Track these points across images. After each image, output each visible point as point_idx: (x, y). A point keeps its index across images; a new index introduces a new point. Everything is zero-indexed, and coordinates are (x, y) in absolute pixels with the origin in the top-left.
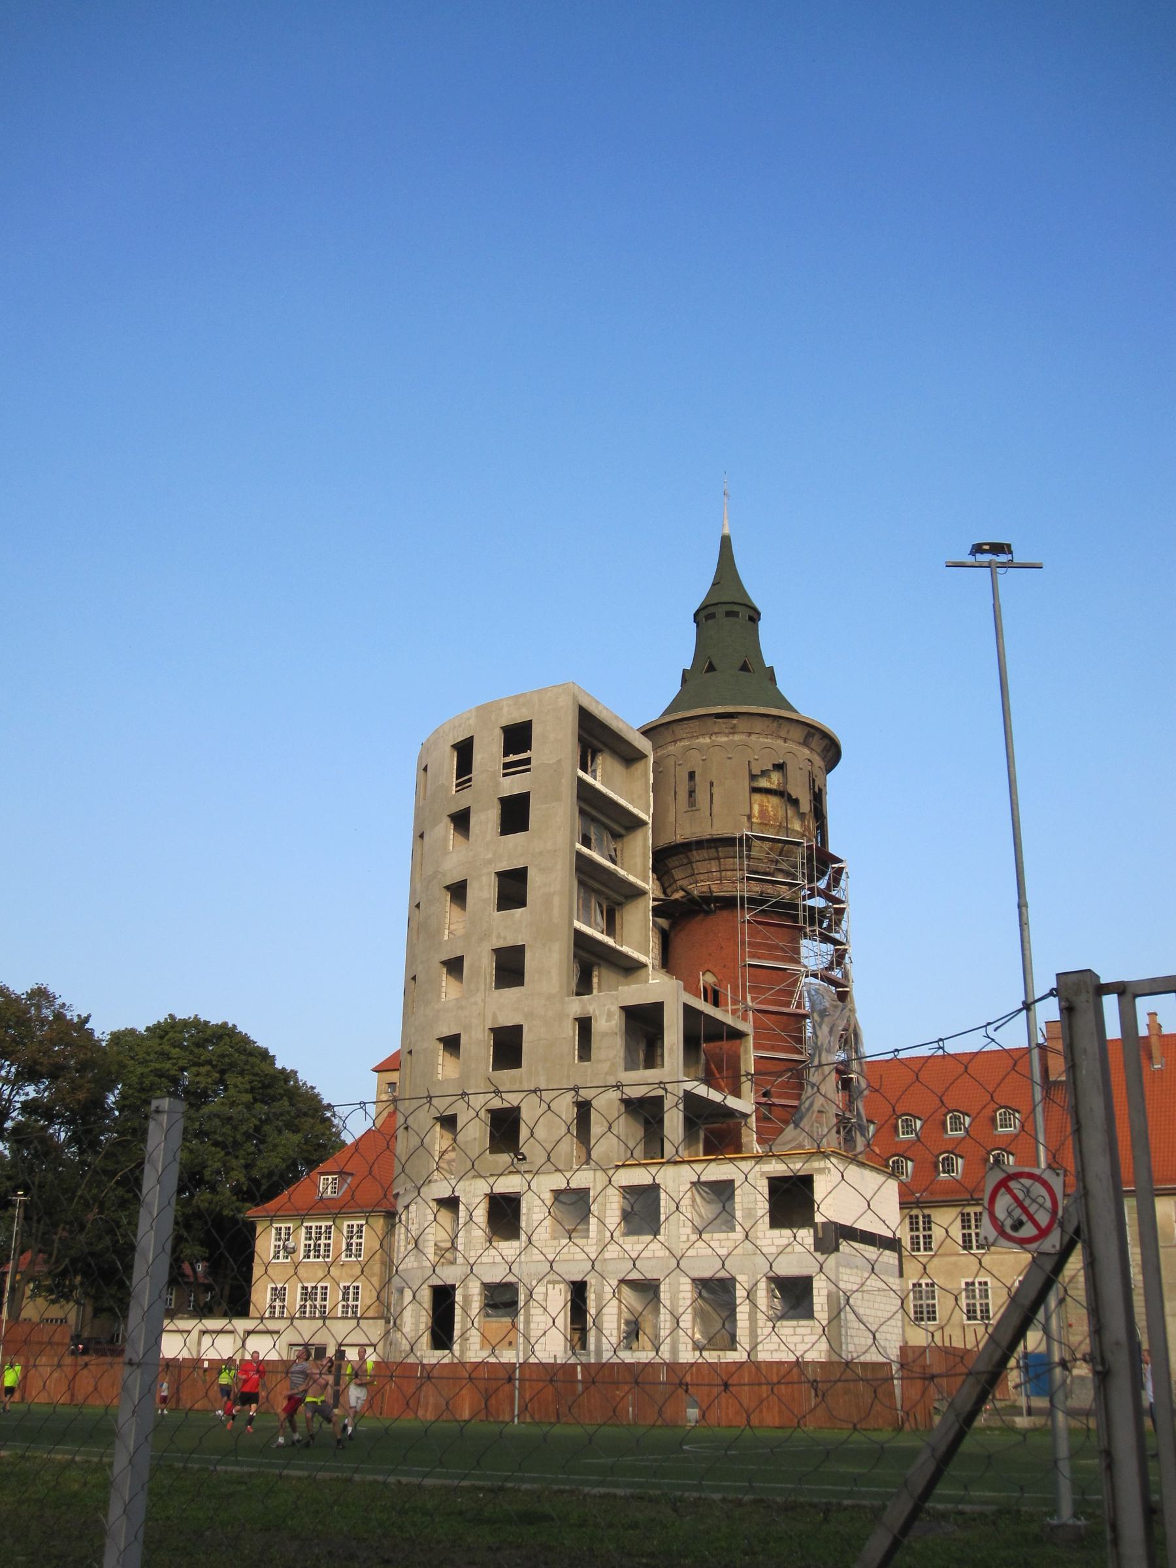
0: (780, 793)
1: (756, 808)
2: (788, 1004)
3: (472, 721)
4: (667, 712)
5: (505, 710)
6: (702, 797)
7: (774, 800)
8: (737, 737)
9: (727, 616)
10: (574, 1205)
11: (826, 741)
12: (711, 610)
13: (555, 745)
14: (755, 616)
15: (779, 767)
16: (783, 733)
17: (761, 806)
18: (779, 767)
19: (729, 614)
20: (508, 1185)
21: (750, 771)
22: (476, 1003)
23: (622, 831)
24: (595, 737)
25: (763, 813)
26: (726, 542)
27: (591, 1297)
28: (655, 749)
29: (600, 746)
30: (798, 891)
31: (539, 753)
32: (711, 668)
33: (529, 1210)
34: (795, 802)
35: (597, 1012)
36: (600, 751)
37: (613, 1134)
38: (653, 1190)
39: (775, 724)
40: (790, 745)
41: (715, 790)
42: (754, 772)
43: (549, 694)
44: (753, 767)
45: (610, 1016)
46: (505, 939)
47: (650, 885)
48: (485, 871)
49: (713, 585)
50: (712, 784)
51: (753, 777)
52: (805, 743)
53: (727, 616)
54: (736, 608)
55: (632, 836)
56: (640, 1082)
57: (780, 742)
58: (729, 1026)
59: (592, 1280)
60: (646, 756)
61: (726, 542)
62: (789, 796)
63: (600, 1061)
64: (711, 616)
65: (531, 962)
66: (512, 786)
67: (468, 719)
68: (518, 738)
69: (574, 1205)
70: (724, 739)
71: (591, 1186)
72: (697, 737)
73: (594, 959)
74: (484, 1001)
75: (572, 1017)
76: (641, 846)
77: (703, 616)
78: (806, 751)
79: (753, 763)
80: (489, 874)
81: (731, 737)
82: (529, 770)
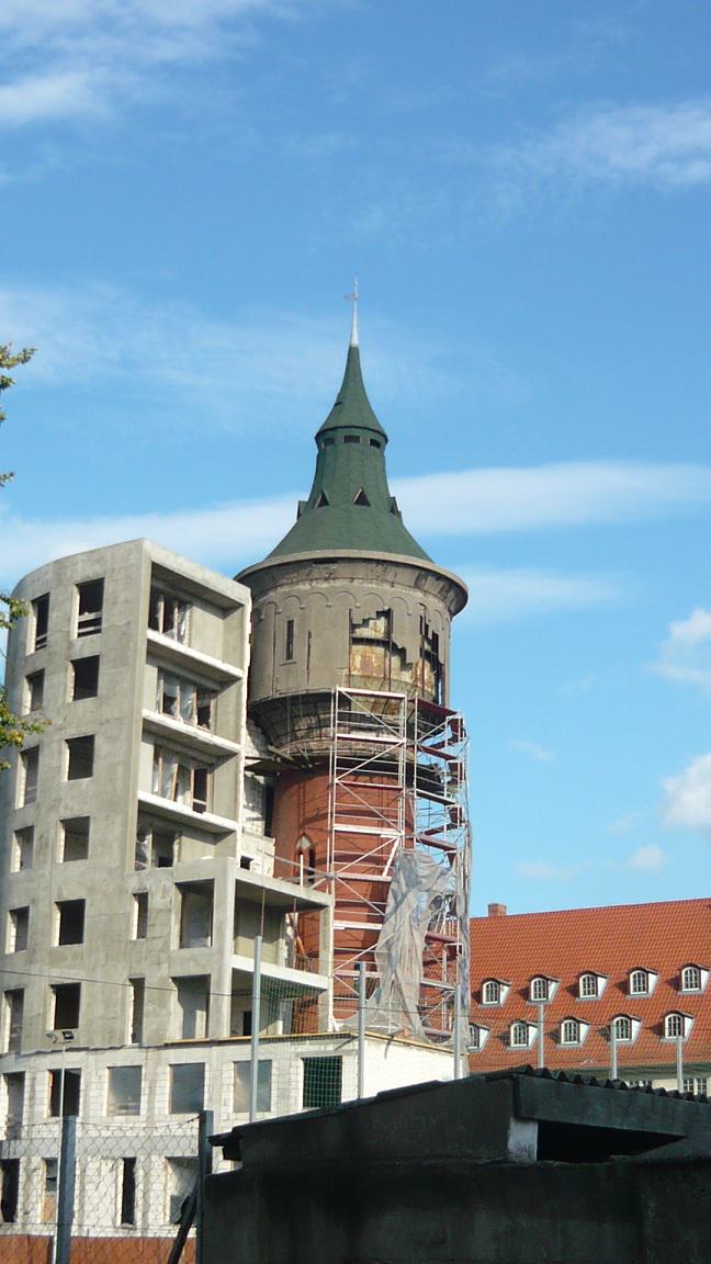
0: (387, 644)
1: (358, 659)
2: (381, 872)
3: (50, 576)
4: (274, 554)
5: (80, 565)
6: (299, 649)
7: (380, 650)
8: (338, 583)
9: (349, 442)
10: (127, 1084)
11: (442, 584)
12: (330, 434)
13: (128, 601)
14: (380, 439)
15: (387, 614)
16: (390, 577)
17: (363, 657)
18: (387, 614)
19: (348, 439)
20: (66, 1061)
21: (351, 620)
22: (43, 875)
23: (216, 687)
24: (173, 593)
25: (365, 663)
26: (353, 355)
27: (139, 1174)
28: (254, 599)
29: (186, 597)
30: (421, 752)
31: (110, 613)
32: (324, 502)
33: (86, 1086)
34: (402, 652)
35: (154, 889)
36: (191, 604)
37: (170, 1015)
38: (198, 1070)
39: (380, 566)
40: (398, 589)
41: (313, 641)
42: (354, 622)
43: (122, 551)
44: (354, 617)
45: (165, 891)
46: (72, 809)
47: (246, 748)
48: (56, 737)
49: (336, 405)
50: (310, 634)
51: (353, 627)
52: (417, 586)
53: (349, 442)
54: (356, 432)
55: (224, 693)
56: (191, 962)
57: (386, 587)
58: (298, 899)
59: (141, 1158)
60: (242, 605)
61: (353, 355)
62: (395, 645)
63: (154, 938)
64: (331, 441)
65: (94, 834)
66: (85, 648)
67: (46, 573)
68: (92, 595)
69: (127, 1084)
70: (325, 585)
71: (143, 1063)
72: (297, 583)
73: (171, 827)
74: (50, 873)
75: (130, 892)
76: (233, 704)
77: (324, 437)
78: (419, 594)
79: (355, 611)
80: (60, 740)
81: (332, 583)
82: (99, 631)
